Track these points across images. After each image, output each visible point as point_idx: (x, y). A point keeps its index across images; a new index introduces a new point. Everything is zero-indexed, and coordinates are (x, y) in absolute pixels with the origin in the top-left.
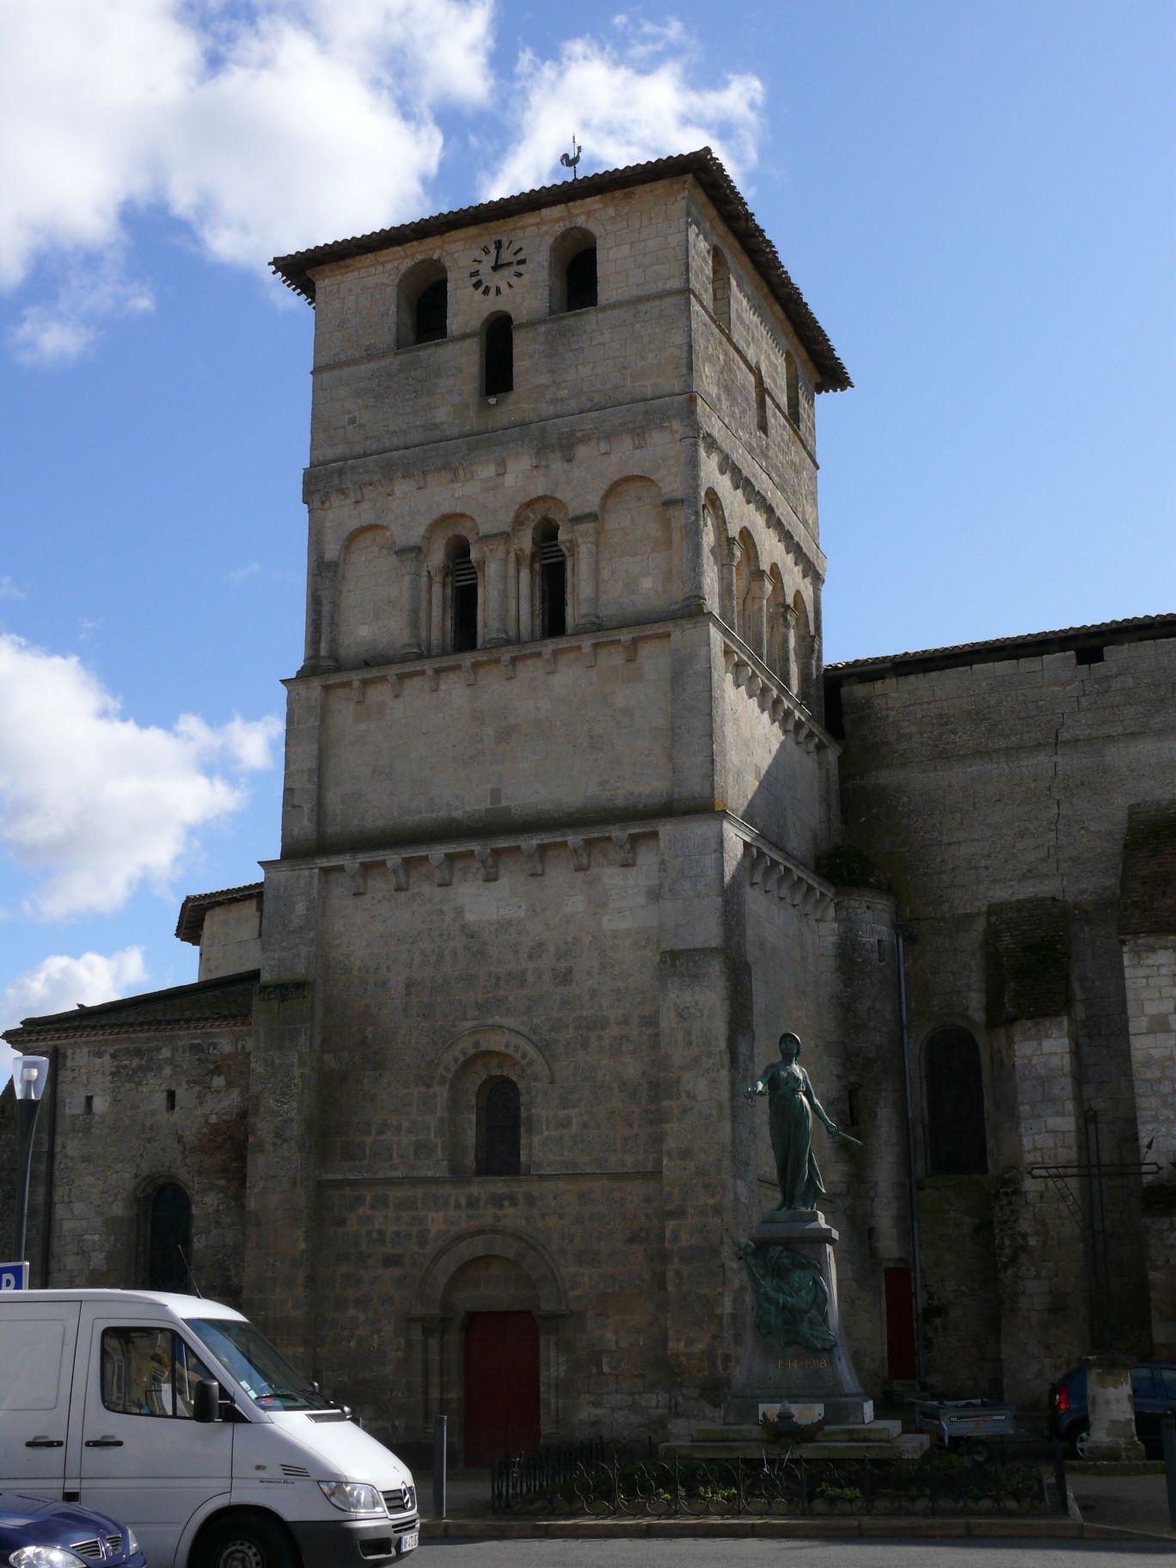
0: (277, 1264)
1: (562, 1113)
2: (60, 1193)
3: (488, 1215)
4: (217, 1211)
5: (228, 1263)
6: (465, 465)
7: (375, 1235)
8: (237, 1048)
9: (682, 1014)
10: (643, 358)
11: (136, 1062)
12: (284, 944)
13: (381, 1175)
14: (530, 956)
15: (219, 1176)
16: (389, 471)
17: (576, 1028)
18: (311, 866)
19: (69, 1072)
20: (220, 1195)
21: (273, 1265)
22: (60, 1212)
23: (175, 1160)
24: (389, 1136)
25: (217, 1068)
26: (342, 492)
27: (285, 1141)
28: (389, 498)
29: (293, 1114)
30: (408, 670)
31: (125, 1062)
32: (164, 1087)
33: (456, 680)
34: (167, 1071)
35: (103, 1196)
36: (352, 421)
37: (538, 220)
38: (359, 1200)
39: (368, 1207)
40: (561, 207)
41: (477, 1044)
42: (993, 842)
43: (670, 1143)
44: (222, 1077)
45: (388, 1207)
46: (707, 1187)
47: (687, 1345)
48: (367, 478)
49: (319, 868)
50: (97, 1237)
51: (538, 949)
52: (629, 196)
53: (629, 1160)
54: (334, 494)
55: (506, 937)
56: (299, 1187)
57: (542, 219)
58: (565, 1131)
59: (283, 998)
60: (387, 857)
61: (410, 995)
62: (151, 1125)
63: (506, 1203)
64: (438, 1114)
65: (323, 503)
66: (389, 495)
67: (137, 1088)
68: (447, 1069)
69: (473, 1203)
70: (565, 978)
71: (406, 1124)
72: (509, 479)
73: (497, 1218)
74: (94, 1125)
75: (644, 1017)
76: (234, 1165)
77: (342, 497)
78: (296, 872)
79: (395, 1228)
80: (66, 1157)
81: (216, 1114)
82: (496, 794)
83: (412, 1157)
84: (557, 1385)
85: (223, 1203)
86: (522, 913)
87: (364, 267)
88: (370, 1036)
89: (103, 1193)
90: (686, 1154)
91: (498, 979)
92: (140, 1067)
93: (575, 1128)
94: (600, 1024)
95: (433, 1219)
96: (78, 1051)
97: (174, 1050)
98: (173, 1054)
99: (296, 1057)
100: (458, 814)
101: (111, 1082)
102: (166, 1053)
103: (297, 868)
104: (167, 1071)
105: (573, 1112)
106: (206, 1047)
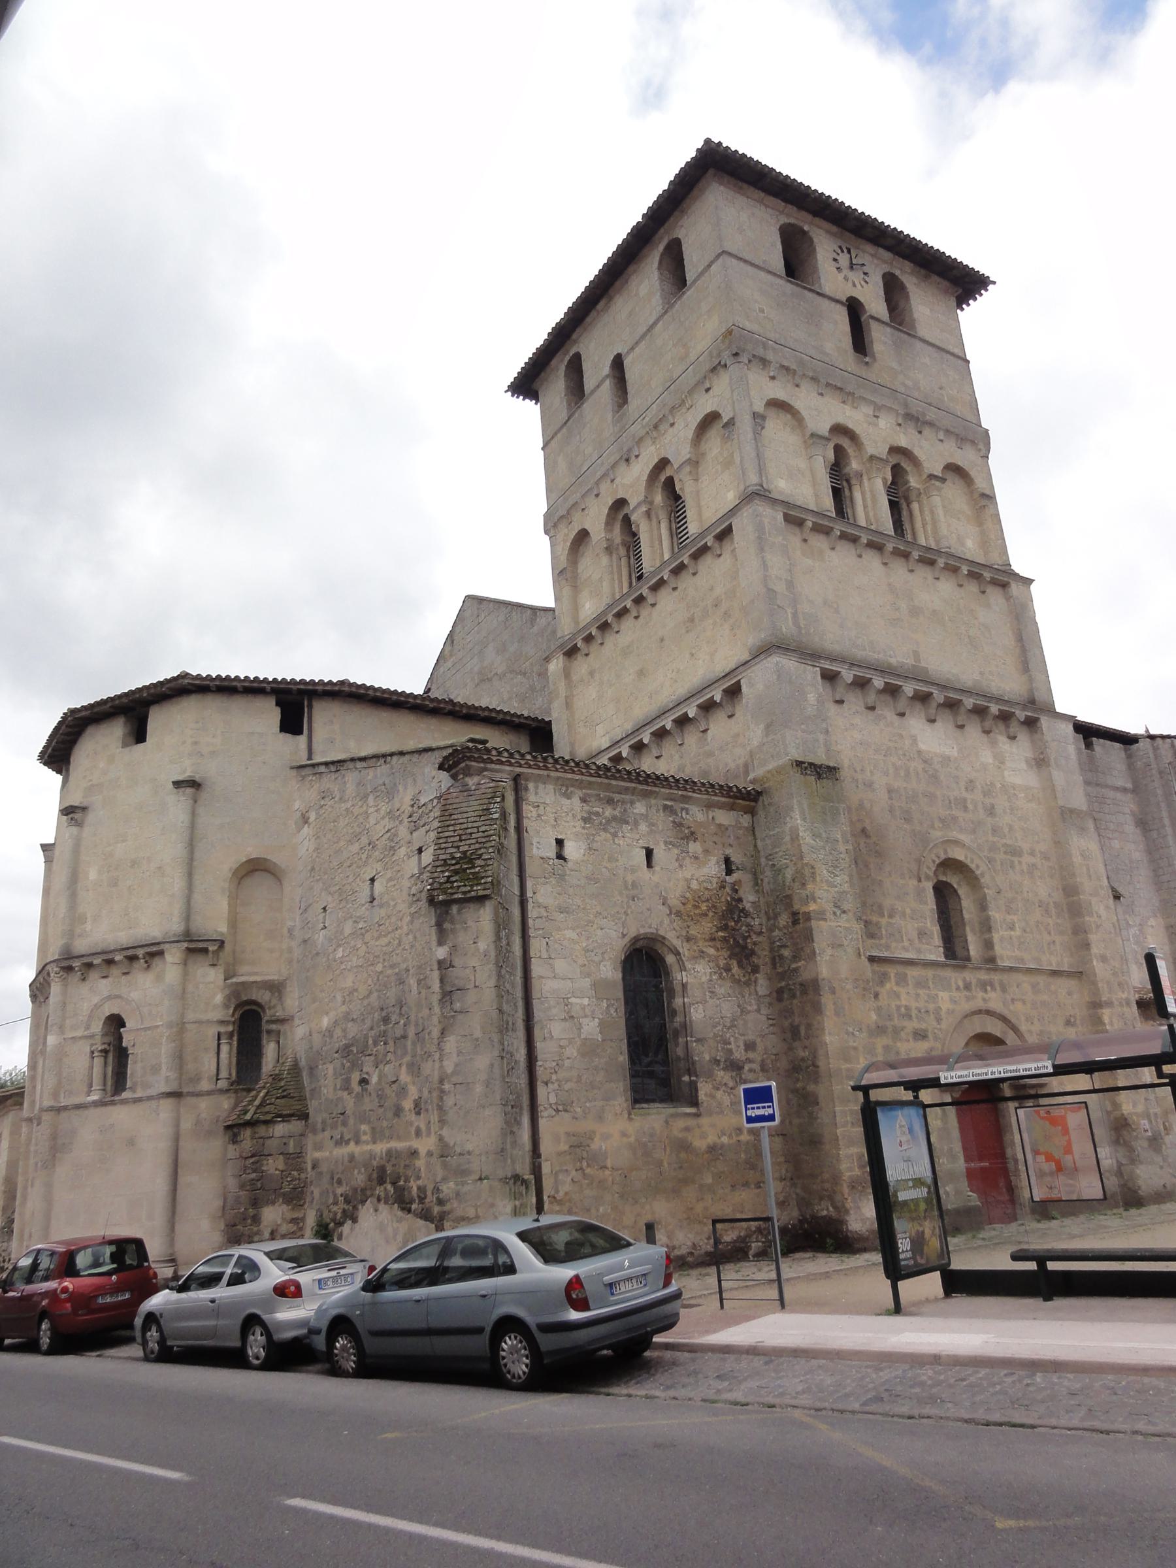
5: (728, 1035)
7: (903, 1010)
12: (803, 727)
14: (967, 789)
21: (853, 1034)
22: (536, 969)
23: (662, 922)
24: (897, 920)
27: (844, 912)
29: (846, 887)
31: (598, 809)
34: (643, 827)
39: (894, 983)
41: (946, 852)
42: (392, 840)
45: (908, 985)
47: (1134, 1106)
49: (822, 669)
50: (586, 1001)
58: (1012, 933)
63: (989, 988)
70: (991, 811)
71: (908, 911)
82: (916, 654)
85: (715, 973)
89: (588, 951)
92: (614, 818)
93: (1018, 932)
94: (1015, 852)
100: (893, 661)
101: (584, 828)
105: (1015, 918)
106: (679, 811)
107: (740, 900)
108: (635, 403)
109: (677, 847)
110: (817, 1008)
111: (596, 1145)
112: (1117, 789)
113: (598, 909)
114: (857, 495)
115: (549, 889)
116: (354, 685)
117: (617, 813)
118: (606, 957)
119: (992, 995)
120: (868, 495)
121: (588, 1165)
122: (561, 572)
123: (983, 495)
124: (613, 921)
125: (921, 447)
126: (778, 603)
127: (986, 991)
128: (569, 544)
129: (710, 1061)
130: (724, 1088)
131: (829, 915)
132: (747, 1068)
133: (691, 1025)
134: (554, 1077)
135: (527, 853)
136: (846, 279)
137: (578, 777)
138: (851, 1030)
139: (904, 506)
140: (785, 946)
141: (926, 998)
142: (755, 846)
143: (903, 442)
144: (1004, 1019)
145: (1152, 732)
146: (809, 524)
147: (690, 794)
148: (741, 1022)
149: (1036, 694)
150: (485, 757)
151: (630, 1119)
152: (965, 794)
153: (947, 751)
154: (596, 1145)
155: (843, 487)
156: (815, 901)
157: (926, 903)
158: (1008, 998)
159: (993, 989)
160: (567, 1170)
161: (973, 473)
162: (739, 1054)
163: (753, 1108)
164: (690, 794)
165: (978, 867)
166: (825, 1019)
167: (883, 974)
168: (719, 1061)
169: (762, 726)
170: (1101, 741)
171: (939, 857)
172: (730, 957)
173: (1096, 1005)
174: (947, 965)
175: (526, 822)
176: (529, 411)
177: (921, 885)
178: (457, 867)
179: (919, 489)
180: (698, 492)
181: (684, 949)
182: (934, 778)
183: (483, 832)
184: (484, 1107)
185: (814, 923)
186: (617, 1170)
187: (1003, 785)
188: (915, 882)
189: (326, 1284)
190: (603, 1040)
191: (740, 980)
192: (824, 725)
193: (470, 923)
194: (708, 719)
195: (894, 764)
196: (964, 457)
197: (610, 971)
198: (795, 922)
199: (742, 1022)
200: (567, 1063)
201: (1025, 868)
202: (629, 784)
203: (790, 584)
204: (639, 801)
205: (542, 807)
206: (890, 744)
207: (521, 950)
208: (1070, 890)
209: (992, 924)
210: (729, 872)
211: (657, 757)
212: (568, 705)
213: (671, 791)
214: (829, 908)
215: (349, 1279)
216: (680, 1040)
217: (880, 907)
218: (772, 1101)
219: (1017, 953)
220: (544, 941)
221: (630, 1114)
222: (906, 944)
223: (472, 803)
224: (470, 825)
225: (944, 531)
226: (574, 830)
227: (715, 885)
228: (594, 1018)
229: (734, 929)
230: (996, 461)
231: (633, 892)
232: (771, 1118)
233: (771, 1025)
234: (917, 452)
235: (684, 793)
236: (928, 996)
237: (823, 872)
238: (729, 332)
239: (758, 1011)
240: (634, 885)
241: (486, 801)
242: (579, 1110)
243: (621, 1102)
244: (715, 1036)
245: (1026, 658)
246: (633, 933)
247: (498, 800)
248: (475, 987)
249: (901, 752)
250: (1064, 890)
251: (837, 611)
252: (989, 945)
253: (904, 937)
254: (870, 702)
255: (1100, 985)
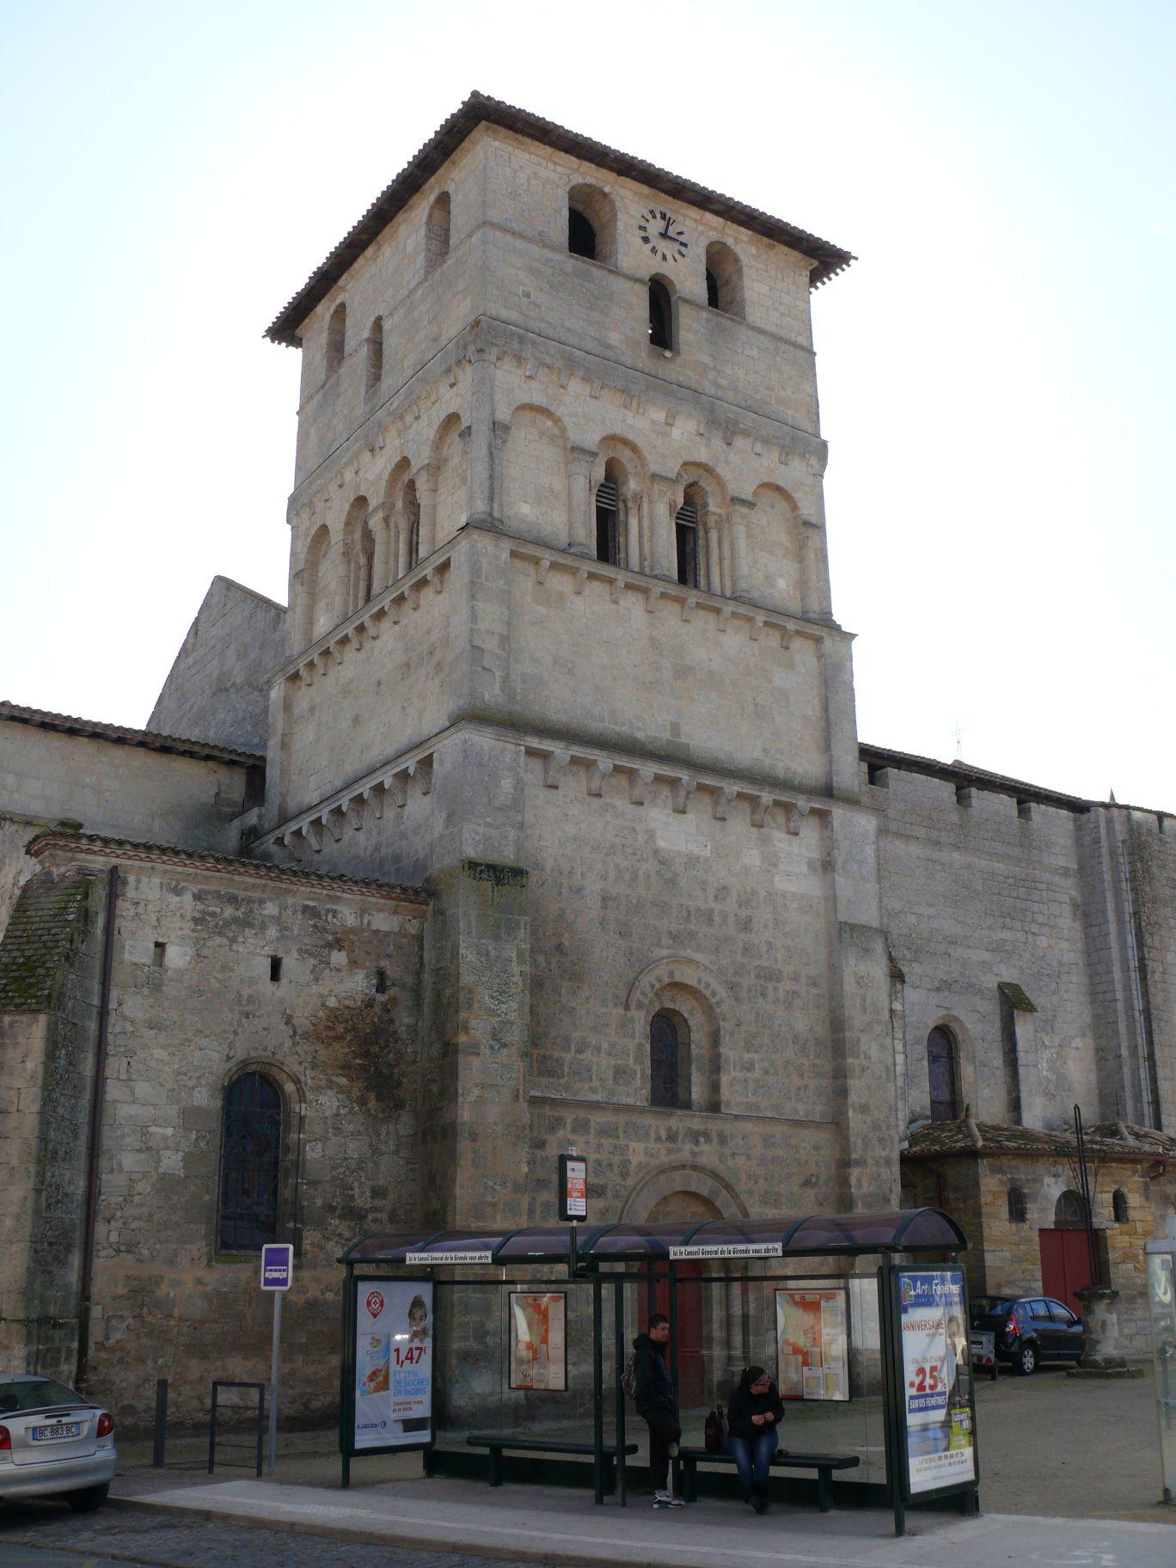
0: (498, 1188)
1: (746, 1056)
2: (116, 1066)
3: (686, 1150)
4: (337, 1115)
5: (350, 1180)
6: (643, 399)
8: (362, 923)
9: (860, 982)
10: (783, 389)
11: (229, 912)
12: (488, 820)
13: (580, 1097)
14: (716, 897)
15: (339, 1071)
16: (571, 365)
17: (757, 976)
18: (519, 742)
19: (128, 905)
20: (341, 1096)
21: (493, 1188)
22: (113, 1091)
23: (282, 1044)
24: (587, 1056)
25: (338, 941)
26: (519, 359)
27: (505, 1046)
28: (562, 390)
30: (601, 572)
32: (267, 950)
33: (635, 601)
34: (272, 932)
35: (179, 1078)
36: (527, 295)
37: (698, 217)
38: (557, 1123)
40: (721, 220)
41: (671, 974)
43: (853, 1098)
44: (343, 953)
45: (589, 1133)
46: (880, 1140)
48: (548, 360)
49: (526, 747)
50: (170, 1131)
51: (722, 892)
52: (771, 247)
53: (801, 1108)
54: (510, 357)
55: (695, 873)
56: (521, 1100)
57: (701, 219)
58: (749, 1074)
59: (498, 882)
60: (599, 758)
61: (606, 908)
62: (250, 996)
63: (702, 1140)
64: (637, 1041)
65: (498, 359)
66: (562, 387)
67: (231, 945)
68: (644, 994)
69: (672, 1137)
70: (746, 925)
71: (605, 1045)
72: (676, 433)
73: (693, 1154)
74: (166, 982)
75: (809, 977)
76: (358, 1061)
77: (515, 365)
78: (501, 743)
79: (596, 1156)
80: (125, 1018)
81: (336, 996)
82: (675, 727)
83: (611, 1081)
84: (39, 1337)
86: (707, 853)
87: (536, 155)
88: (566, 943)
90: (864, 1109)
91: (689, 913)
92: (235, 920)
93: (757, 1074)
94: (772, 976)
95: (634, 1150)
96: (145, 880)
97: (283, 907)
98: (280, 912)
99: (515, 951)
100: (641, 735)
101: (193, 931)
102: (271, 909)
103: (503, 738)
104: (272, 932)
105: (756, 1056)
106: (323, 912)
107: (391, 1021)
108: (387, 382)
109: (315, 957)
110: (452, 1156)
111: (163, 1291)
112: (1055, 871)
113: (199, 1026)
114: (633, 523)
115: (139, 999)
116: (16, 707)
117: (239, 914)
118: (203, 1082)
119: (704, 1147)
120: (646, 523)
121: (150, 1313)
122: (297, 574)
123: (807, 524)
124: (217, 1041)
125: (727, 463)
126: (485, 663)
127: (697, 1143)
128: (309, 539)
129: (323, 1207)
130: (337, 1239)
131: (485, 1050)
132: (370, 1218)
133: (304, 1164)
134: (119, 1214)
135: (116, 957)
136: (654, 250)
137: (191, 871)
138: (490, 1183)
139: (701, 534)
140: (434, 1081)
141: (612, 1149)
142: (422, 957)
143: (702, 456)
144: (716, 1176)
145: (1120, 801)
146: (546, 564)
147: (339, 894)
148: (371, 1165)
149: (835, 778)
150: (73, 845)
151: (209, 1265)
152: (712, 904)
153: (696, 850)
154: (163, 1291)
155: (618, 509)
156: (467, 1032)
157: (632, 1036)
158: (728, 1151)
159: (708, 1140)
160: (122, 1316)
161: (797, 496)
162: (362, 1200)
163: (271, 1270)
164: (339, 894)
165: (714, 994)
166: (458, 1169)
167: (556, 1120)
168: (336, 1207)
169: (444, 815)
170: (1043, 807)
171: (660, 981)
172: (367, 1089)
173: (844, 1164)
174: (649, 1112)
175: (118, 922)
176: (290, 359)
177: (630, 1014)
178: (17, 974)
179: (720, 516)
180: (435, 507)
181: (309, 1077)
182: (672, 883)
183: (54, 935)
184: (12, 1242)
185: (461, 1059)
186: (187, 1321)
187: (769, 894)
188: (621, 1010)
189: (42, 1433)
190: (187, 1177)
191: (377, 1117)
192: (520, 818)
193: (21, 1039)
194: (381, 802)
195: (617, 866)
196: (791, 474)
197: (205, 1098)
198: (445, 1054)
199: (371, 1165)
200: (137, 1199)
201: (781, 994)
202: (257, 881)
203: (505, 640)
204: (271, 900)
205: (142, 904)
206: (616, 840)
207: (94, 1070)
208: (837, 1024)
209: (723, 1063)
210: (381, 988)
211: (357, 829)
212: (284, 746)
213: (314, 890)
214: (485, 1041)
215: (73, 1430)
216: (290, 1181)
217: (567, 1039)
218: (287, 1265)
219: (752, 1099)
220: (125, 1061)
221: (210, 1260)
222: (595, 1083)
223: (53, 899)
224: (42, 925)
225: (744, 569)
226: (180, 933)
227: (359, 1004)
228: (178, 1151)
229: (377, 1057)
230: (833, 482)
231: (248, 1008)
232: (283, 1282)
233: (411, 1170)
234: (721, 470)
235: (331, 893)
236: (615, 1147)
237: (485, 997)
238: (477, 323)
239: (397, 1152)
240: (250, 999)
241: (66, 898)
242: (146, 1252)
243: (199, 1248)
244: (333, 1179)
245: (829, 732)
246: (240, 1054)
247: (79, 897)
248: (18, 1111)
249: (629, 851)
250: (831, 1023)
251: (571, 672)
252: (715, 1087)
253: (594, 1077)
254: (596, 784)
255: (852, 1139)
